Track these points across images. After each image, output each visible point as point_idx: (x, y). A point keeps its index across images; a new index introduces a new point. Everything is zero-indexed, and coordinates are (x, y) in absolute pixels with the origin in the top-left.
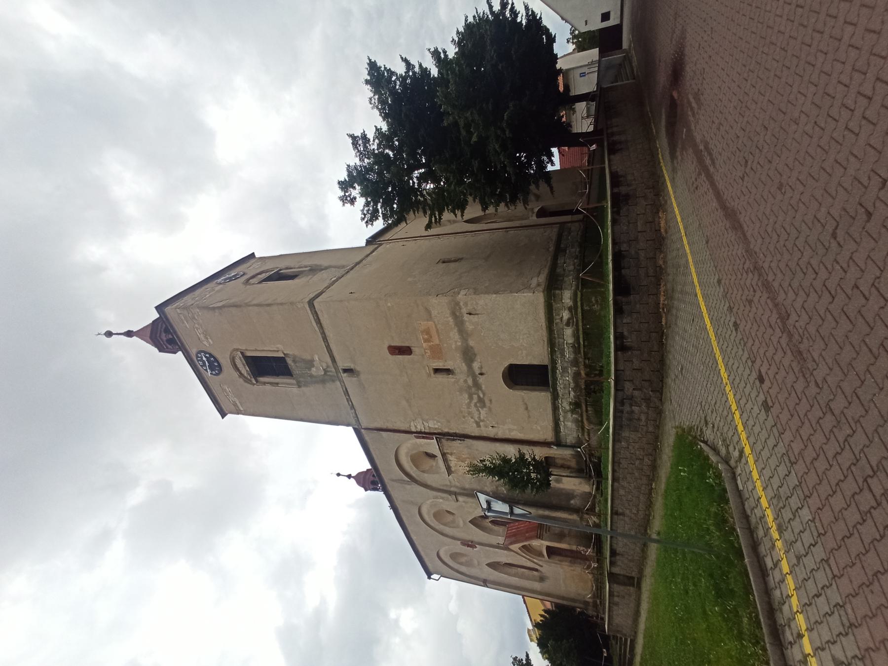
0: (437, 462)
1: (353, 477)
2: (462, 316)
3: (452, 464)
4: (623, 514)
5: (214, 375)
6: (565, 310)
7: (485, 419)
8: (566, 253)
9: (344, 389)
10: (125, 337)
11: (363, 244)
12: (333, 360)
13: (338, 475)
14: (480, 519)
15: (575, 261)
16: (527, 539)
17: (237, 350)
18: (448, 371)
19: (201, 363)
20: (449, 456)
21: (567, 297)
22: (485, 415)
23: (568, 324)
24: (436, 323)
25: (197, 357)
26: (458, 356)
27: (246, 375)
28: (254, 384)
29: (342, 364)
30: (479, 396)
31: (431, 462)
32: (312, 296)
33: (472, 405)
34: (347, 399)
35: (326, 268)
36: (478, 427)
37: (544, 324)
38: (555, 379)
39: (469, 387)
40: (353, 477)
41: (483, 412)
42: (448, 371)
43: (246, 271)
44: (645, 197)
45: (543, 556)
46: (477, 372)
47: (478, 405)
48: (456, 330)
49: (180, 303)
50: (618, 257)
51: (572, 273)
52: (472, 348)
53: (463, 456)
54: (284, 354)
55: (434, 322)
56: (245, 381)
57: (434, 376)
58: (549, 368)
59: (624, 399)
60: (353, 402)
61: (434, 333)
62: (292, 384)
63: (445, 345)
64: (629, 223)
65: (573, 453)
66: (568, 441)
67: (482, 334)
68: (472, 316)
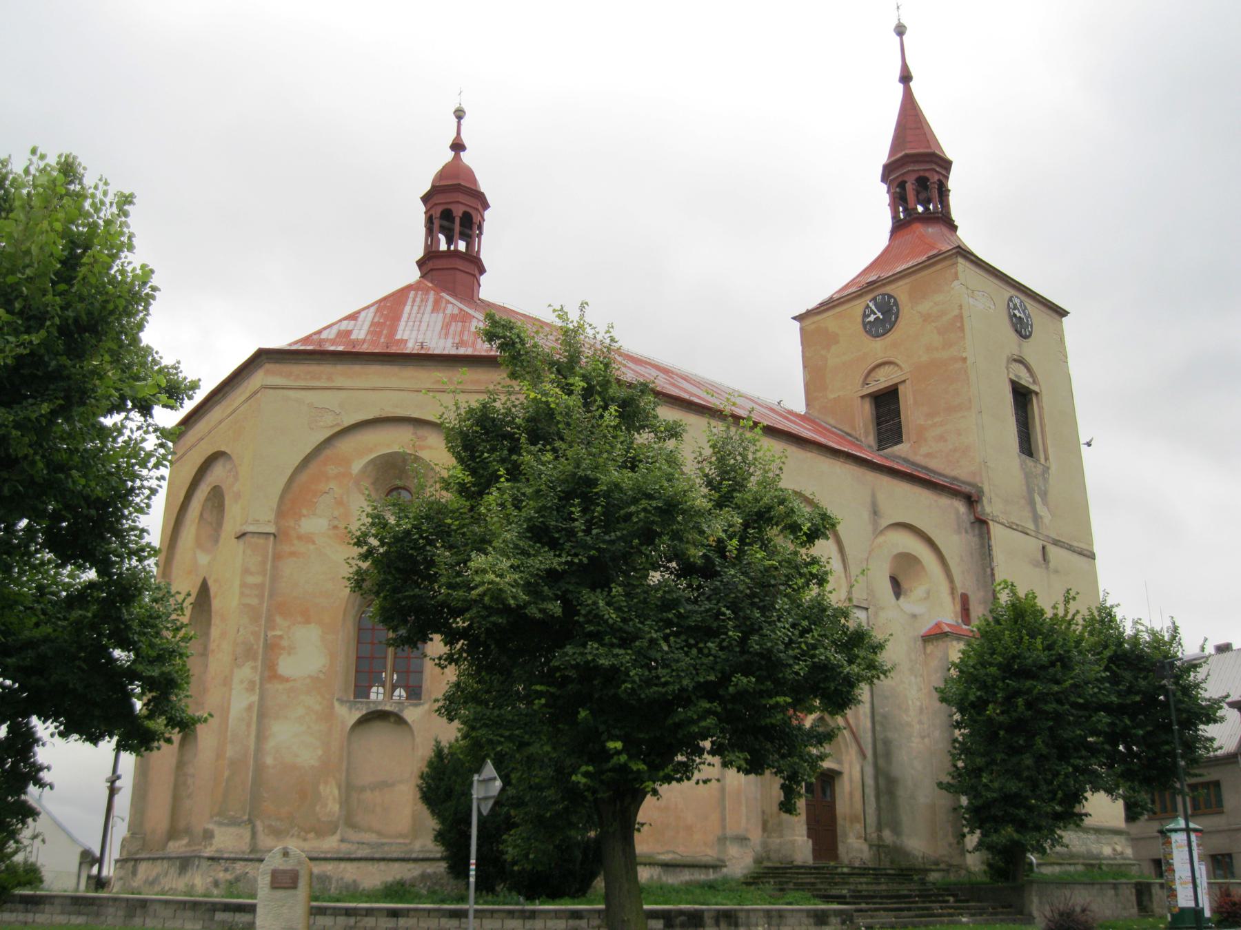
1: (457, 157)
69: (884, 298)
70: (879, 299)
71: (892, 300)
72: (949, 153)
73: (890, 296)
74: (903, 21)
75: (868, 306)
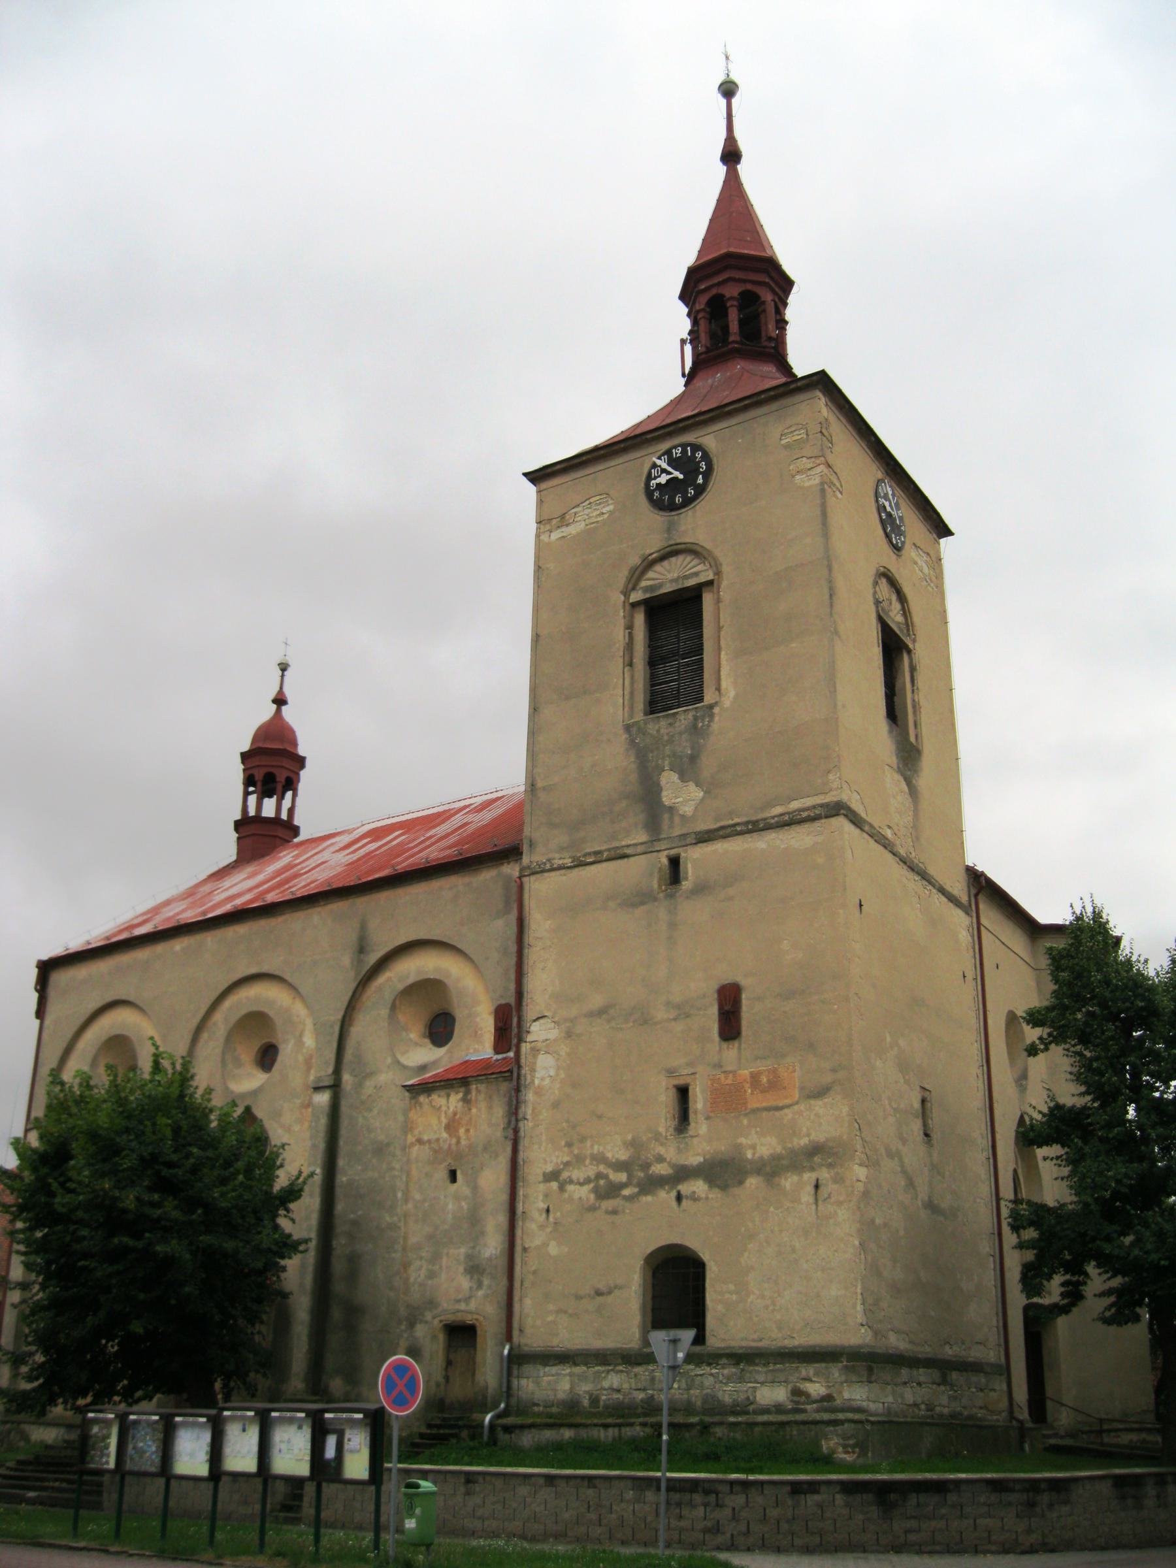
0: (417, 1044)
1: (278, 711)
2: (812, 1169)
3: (438, 1099)
7: (566, 1195)
9: (628, 851)
12: (705, 837)
13: (284, 667)
15: (923, 1407)
17: (718, 573)
20: (461, 1095)
21: (856, 1394)
23: (797, 1392)
24: (796, 1107)
26: (721, 1147)
27: (650, 574)
28: (626, 594)
29: (695, 859)
30: (623, 1186)
32: (856, 806)
35: (913, 792)
36: (545, 1175)
37: (796, 1343)
39: (646, 1166)
41: (583, 1193)
44: (1029, 1531)
46: (685, 1188)
47: (602, 1182)
48: (779, 1149)
49: (839, 429)
50: (940, 1487)
51: (900, 1401)
55: (797, 1103)
56: (633, 571)
57: (670, 1086)
59: (717, 1495)
60: (593, 867)
61: (771, 1100)
62: (632, 708)
63: (745, 1122)
64: (989, 1505)
65: (490, 1391)
67: (772, 1209)
68: (813, 1191)
69: (684, 452)
70: (677, 452)
71: (699, 455)
72: (789, 266)
73: (696, 447)
75: (654, 466)
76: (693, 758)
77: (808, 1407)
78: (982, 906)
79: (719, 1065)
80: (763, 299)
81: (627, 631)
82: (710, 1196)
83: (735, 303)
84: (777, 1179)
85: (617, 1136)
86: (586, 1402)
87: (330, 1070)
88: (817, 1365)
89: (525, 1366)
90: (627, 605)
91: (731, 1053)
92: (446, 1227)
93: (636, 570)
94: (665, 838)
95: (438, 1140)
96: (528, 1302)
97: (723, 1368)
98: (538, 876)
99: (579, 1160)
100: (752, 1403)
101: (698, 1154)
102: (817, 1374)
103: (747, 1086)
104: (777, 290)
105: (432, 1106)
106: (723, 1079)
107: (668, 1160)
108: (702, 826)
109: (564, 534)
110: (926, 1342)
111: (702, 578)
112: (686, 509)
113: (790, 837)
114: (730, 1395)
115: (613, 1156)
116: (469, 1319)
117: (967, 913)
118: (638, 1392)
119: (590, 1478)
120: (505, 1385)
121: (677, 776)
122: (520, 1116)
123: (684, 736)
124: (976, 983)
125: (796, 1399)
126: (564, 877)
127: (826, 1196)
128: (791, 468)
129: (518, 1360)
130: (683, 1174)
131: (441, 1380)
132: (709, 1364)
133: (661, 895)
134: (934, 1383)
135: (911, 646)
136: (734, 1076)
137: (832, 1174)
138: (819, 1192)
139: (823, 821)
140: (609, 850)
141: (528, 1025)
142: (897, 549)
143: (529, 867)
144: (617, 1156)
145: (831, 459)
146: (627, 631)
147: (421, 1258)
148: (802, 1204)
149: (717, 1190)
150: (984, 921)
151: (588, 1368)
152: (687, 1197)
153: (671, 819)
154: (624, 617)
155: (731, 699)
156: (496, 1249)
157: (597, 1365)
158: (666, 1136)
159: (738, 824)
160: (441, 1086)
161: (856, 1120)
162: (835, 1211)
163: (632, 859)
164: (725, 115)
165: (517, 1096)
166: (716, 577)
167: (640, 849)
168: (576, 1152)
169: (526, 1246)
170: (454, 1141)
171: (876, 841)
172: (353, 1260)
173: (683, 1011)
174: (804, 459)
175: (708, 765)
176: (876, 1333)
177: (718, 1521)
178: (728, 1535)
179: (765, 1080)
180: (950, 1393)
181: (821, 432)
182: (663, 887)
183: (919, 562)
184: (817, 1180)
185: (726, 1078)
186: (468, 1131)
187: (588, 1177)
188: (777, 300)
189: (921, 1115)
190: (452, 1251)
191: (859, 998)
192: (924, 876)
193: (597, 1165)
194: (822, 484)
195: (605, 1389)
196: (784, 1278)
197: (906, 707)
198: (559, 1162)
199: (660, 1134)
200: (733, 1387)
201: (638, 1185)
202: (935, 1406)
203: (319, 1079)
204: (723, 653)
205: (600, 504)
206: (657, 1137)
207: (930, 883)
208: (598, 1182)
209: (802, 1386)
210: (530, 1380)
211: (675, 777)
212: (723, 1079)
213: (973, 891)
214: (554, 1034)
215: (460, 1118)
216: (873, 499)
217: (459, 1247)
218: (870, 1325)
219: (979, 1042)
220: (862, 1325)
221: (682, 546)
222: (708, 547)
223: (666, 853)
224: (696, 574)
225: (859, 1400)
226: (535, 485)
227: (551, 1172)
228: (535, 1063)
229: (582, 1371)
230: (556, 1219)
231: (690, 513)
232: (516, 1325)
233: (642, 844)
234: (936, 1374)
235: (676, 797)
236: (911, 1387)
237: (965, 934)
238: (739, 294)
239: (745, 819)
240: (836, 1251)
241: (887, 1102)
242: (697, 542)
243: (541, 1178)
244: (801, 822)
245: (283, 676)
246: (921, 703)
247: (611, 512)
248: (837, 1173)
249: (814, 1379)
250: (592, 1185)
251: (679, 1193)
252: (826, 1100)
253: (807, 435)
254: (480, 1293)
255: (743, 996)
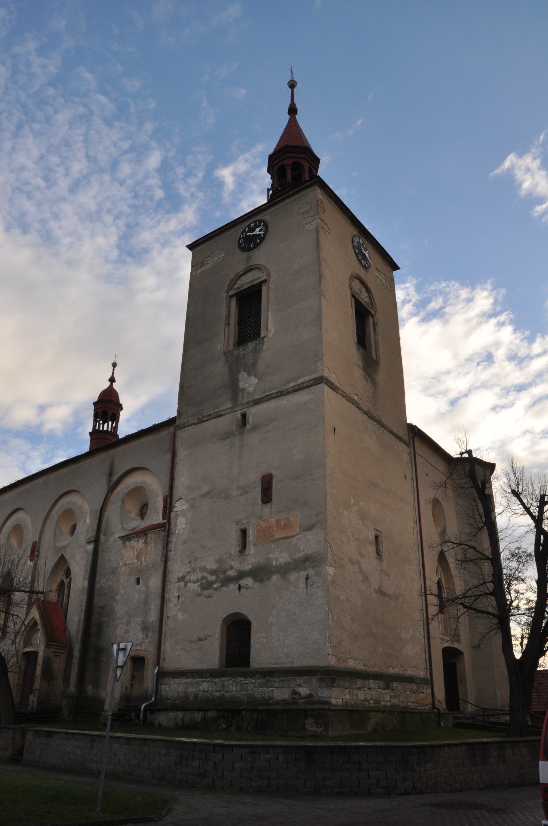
0: (134, 519)
1: (111, 386)
2: (305, 569)
3: (134, 543)
4: (92, 747)
5: (239, 241)
6: (310, 690)
7: (187, 589)
8: (384, 689)
9: (222, 413)
10: (288, 105)
11: (409, 421)
12: (258, 402)
14: (65, 568)
16: (45, 627)
17: (269, 276)
18: (244, 546)
19: (253, 225)
20: (143, 540)
22: (192, 589)
23: (294, 693)
25: (260, 221)
27: (239, 282)
28: (227, 292)
30: (214, 582)
31: (134, 513)
32: (333, 378)
33: (204, 574)
34: (210, 415)
38: (234, 675)
39: (225, 572)
40: (111, 386)
41: (194, 587)
42: (244, 546)
43: (371, 270)
45: (25, 647)
46: (243, 582)
47: (204, 581)
48: (289, 560)
52: (269, 578)
53: (143, 558)
54: (263, 338)
55: (298, 534)
56: (231, 281)
57: (238, 530)
58: (245, 669)
62: (228, 345)
63: (273, 546)
66: (164, 687)
67: (284, 592)
74: (294, 79)
76: (254, 364)
77: (300, 701)
78: (416, 444)
79: (261, 517)
80: (303, 165)
81: (227, 309)
82: (254, 586)
83: (290, 167)
84: (287, 576)
85: (211, 557)
86: (192, 697)
87: (94, 533)
88: (304, 677)
89: (165, 678)
90: (228, 297)
91: (267, 509)
92: (134, 607)
93: (232, 281)
94: (240, 405)
95: (133, 563)
96: (168, 645)
97: (258, 679)
98: (182, 430)
99: (194, 570)
100: (271, 699)
101: (249, 564)
102: (305, 682)
103: (274, 526)
104: (310, 161)
105: (131, 546)
106: (262, 524)
107: (235, 568)
108: (257, 397)
109: (203, 270)
110: (375, 666)
111: (261, 279)
112: (255, 249)
113: (298, 397)
114: (261, 694)
115: (210, 567)
116: (141, 654)
117: (407, 446)
118: (216, 692)
119: (145, 740)
120: (155, 688)
121: (246, 373)
122: (169, 549)
123: (250, 354)
124: (413, 481)
125: (294, 696)
126: (194, 429)
127: (312, 583)
128: (303, 222)
129: (162, 675)
130: (242, 575)
131: (129, 686)
132: (251, 677)
133: (237, 433)
134: (380, 688)
135: (373, 313)
136: (268, 522)
137: (315, 571)
138: (308, 581)
139: (314, 387)
140: (214, 413)
141: (174, 503)
142: (366, 268)
143: (178, 426)
144: (211, 567)
145: (323, 217)
146: (227, 309)
147: (122, 623)
148: (300, 588)
149: (258, 583)
150: (417, 450)
151: (193, 679)
152: (243, 587)
153: (243, 394)
154: (226, 303)
155: (272, 333)
156: (155, 617)
157: (198, 678)
158: (235, 556)
159: (274, 393)
160: (135, 536)
161: (328, 542)
162: (316, 592)
163: (224, 417)
164: (290, 95)
165: (167, 539)
166: (268, 278)
167: (228, 411)
168: (193, 566)
169: (168, 616)
170: (140, 563)
171: (346, 400)
172: (100, 625)
173: (245, 491)
174: (309, 217)
175: (261, 367)
176: (339, 660)
177: (206, 769)
178: (211, 779)
179: (283, 523)
180: (392, 694)
181: (317, 204)
182: (238, 429)
183: (380, 278)
184: (307, 575)
185: (264, 523)
186: (146, 558)
187: (198, 579)
188: (311, 166)
189: (375, 544)
190: (135, 619)
191: (332, 477)
192: (379, 423)
193: (202, 573)
194: (317, 227)
195: (201, 691)
196: (289, 629)
197: (371, 343)
198: (185, 572)
199: (232, 555)
200: (262, 690)
201: (221, 582)
202: (381, 701)
203: (90, 538)
204: (270, 312)
205: (219, 254)
206: (230, 556)
207: (383, 427)
208: (202, 581)
209: (297, 690)
210: (167, 686)
211: (245, 374)
212: (262, 524)
213: (411, 436)
214: (185, 507)
215: (143, 552)
216: (350, 243)
217: (139, 617)
218: (335, 654)
219: (414, 510)
220: (329, 655)
221: (253, 267)
222: (264, 265)
223: (240, 412)
224: (259, 278)
225: (326, 697)
226: (191, 251)
227: (181, 577)
228: (176, 522)
229: (190, 681)
230: (182, 601)
231: (257, 251)
232: (162, 657)
233: (229, 409)
234: (382, 684)
235: (246, 384)
236: (364, 691)
237: (406, 456)
238: (292, 163)
239: (277, 391)
240: (316, 614)
241: (350, 534)
242: (260, 263)
243: (176, 580)
244: (303, 388)
245: (114, 370)
246: (379, 340)
247: (223, 257)
248: (318, 571)
249: (303, 685)
250: (199, 583)
251: (239, 585)
252: (313, 531)
253: (311, 207)
254: (147, 641)
255: (274, 480)
